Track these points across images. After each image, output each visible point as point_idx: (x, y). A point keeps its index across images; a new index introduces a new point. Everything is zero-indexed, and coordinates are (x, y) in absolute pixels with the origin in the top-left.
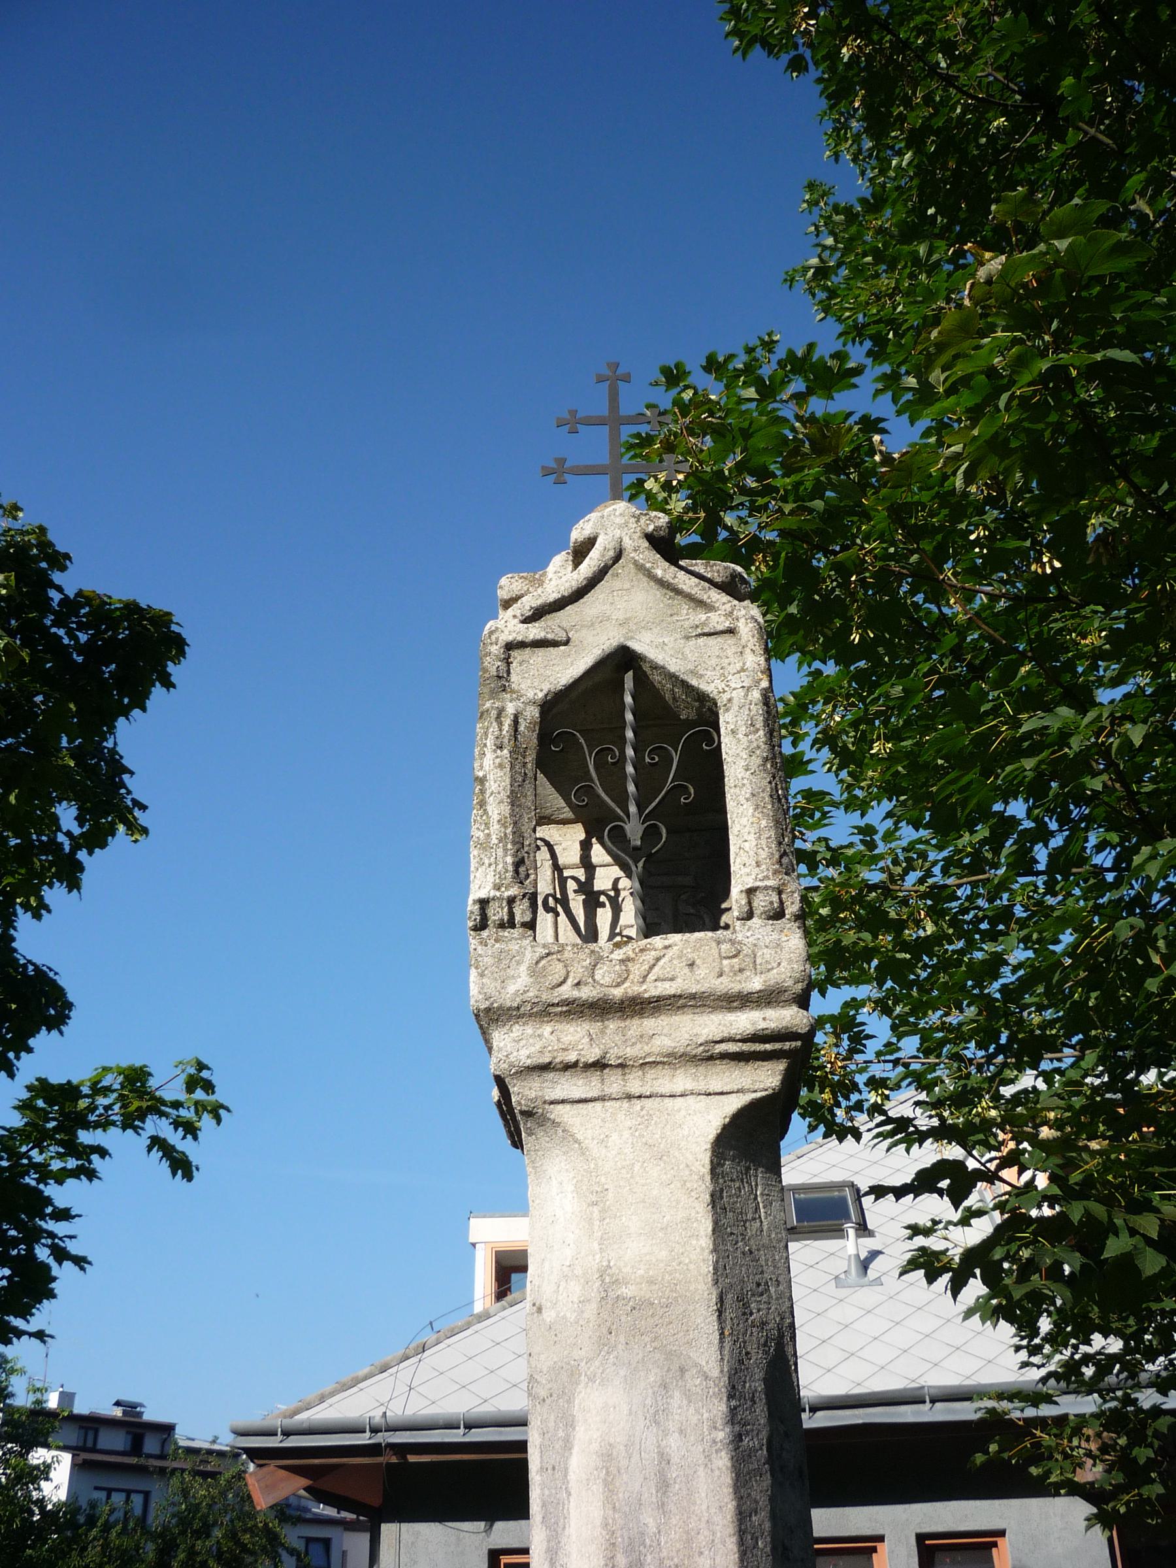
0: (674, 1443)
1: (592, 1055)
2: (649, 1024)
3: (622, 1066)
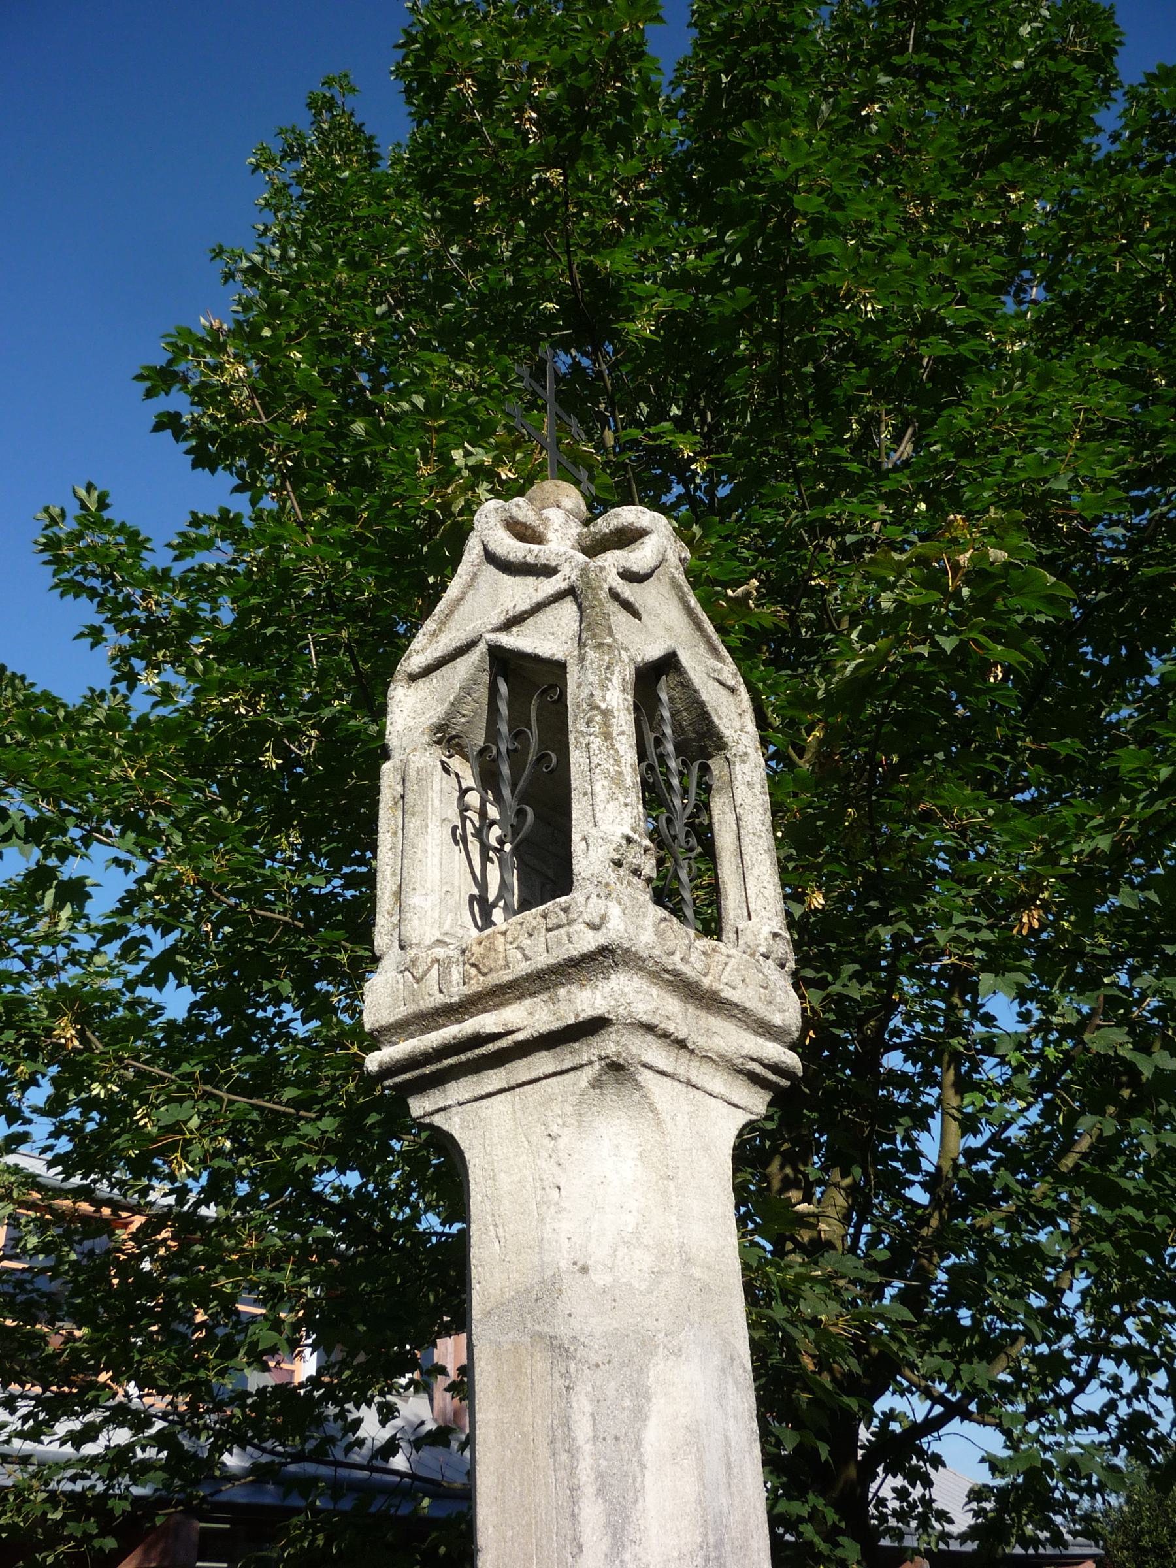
2: (716, 1023)
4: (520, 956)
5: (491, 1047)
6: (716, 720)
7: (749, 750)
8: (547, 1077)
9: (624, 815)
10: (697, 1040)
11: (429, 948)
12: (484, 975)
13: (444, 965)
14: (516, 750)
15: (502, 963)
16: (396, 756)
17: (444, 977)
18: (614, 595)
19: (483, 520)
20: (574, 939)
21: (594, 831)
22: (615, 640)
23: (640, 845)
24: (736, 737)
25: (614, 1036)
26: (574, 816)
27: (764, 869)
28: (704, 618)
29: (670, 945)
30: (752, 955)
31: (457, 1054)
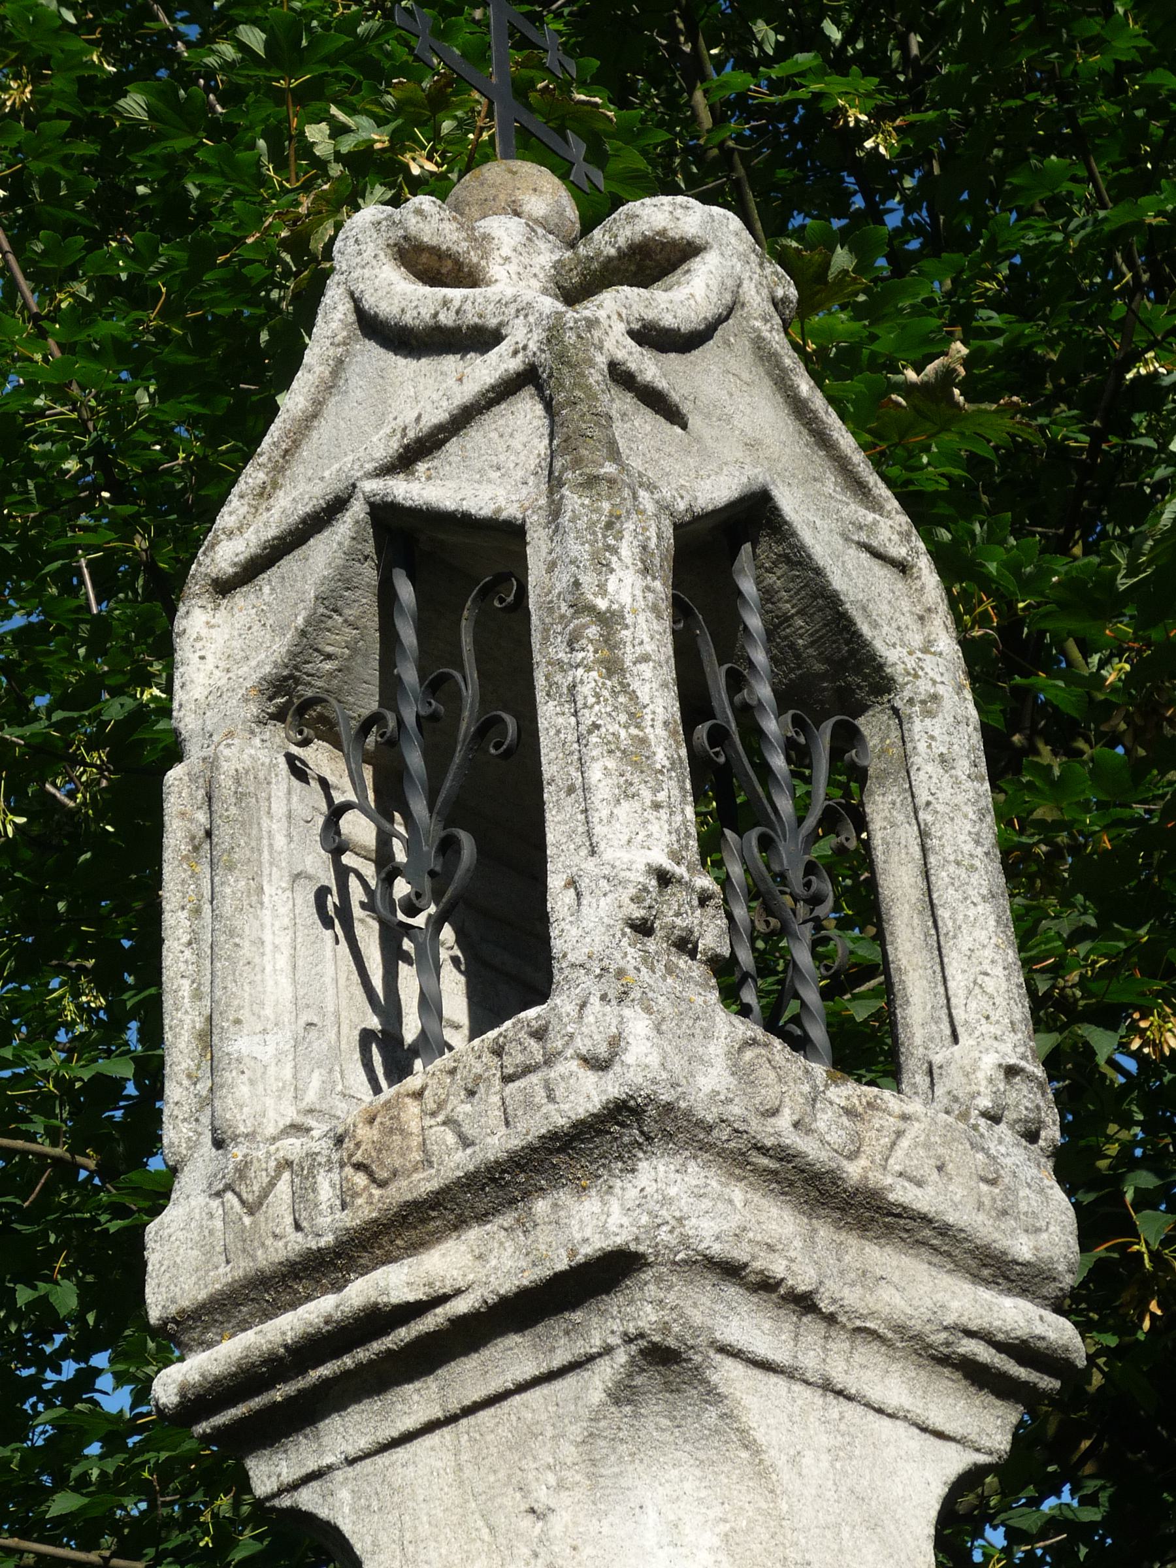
1: (803, 1279)
2: (881, 1257)
3: (831, 1319)
4: (451, 1138)
5: (404, 1334)
6: (865, 629)
7: (941, 690)
8: (522, 1387)
9: (654, 828)
10: (838, 1293)
11: (274, 1139)
12: (382, 1184)
13: (302, 1171)
14: (434, 717)
15: (416, 1156)
16: (195, 752)
17: (303, 1196)
18: (620, 376)
19: (352, 248)
20: (559, 1093)
21: (590, 865)
22: (624, 468)
23: (689, 887)
24: (911, 663)
25: (652, 1290)
26: (550, 838)
27: (982, 936)
28: (832, 419)
29: (769, 1095)
30: (964, 1116)
31: (337, 1355)
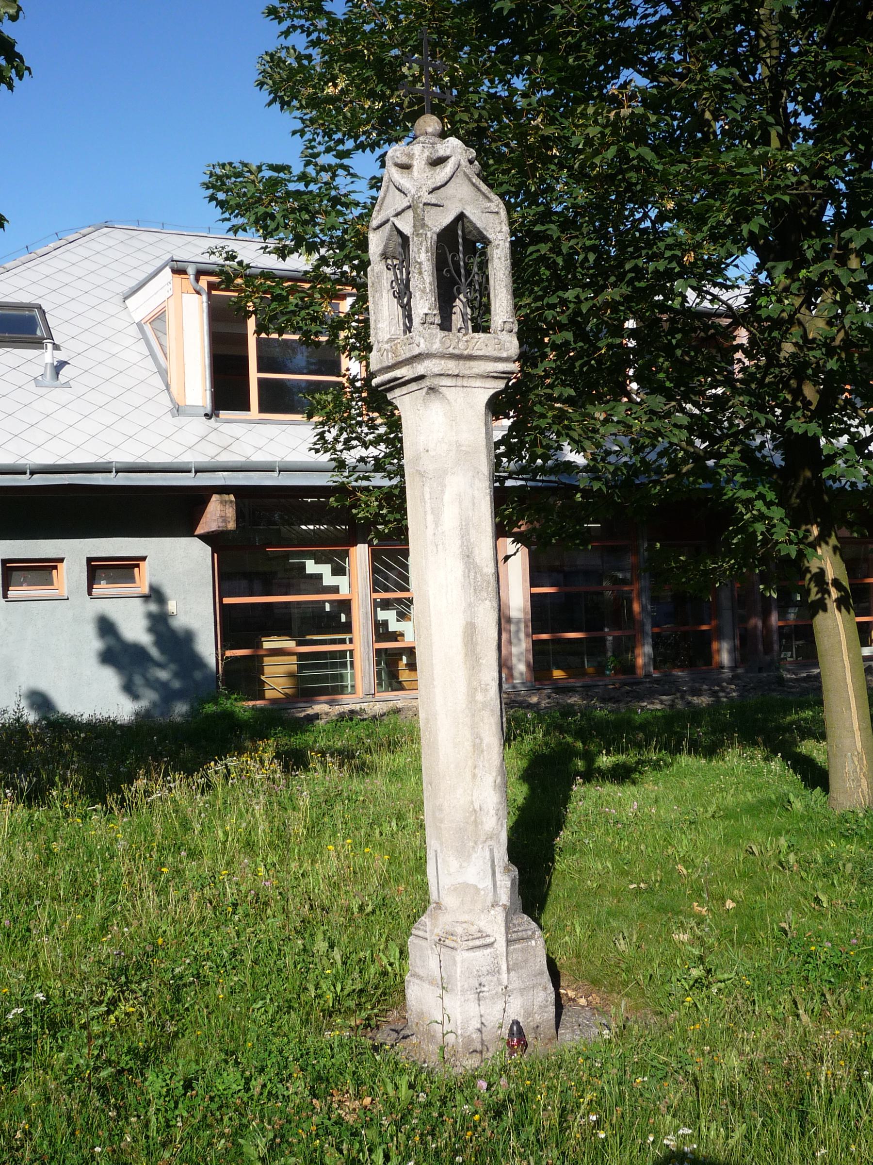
0: (476, 493)
2: (472, 363)
